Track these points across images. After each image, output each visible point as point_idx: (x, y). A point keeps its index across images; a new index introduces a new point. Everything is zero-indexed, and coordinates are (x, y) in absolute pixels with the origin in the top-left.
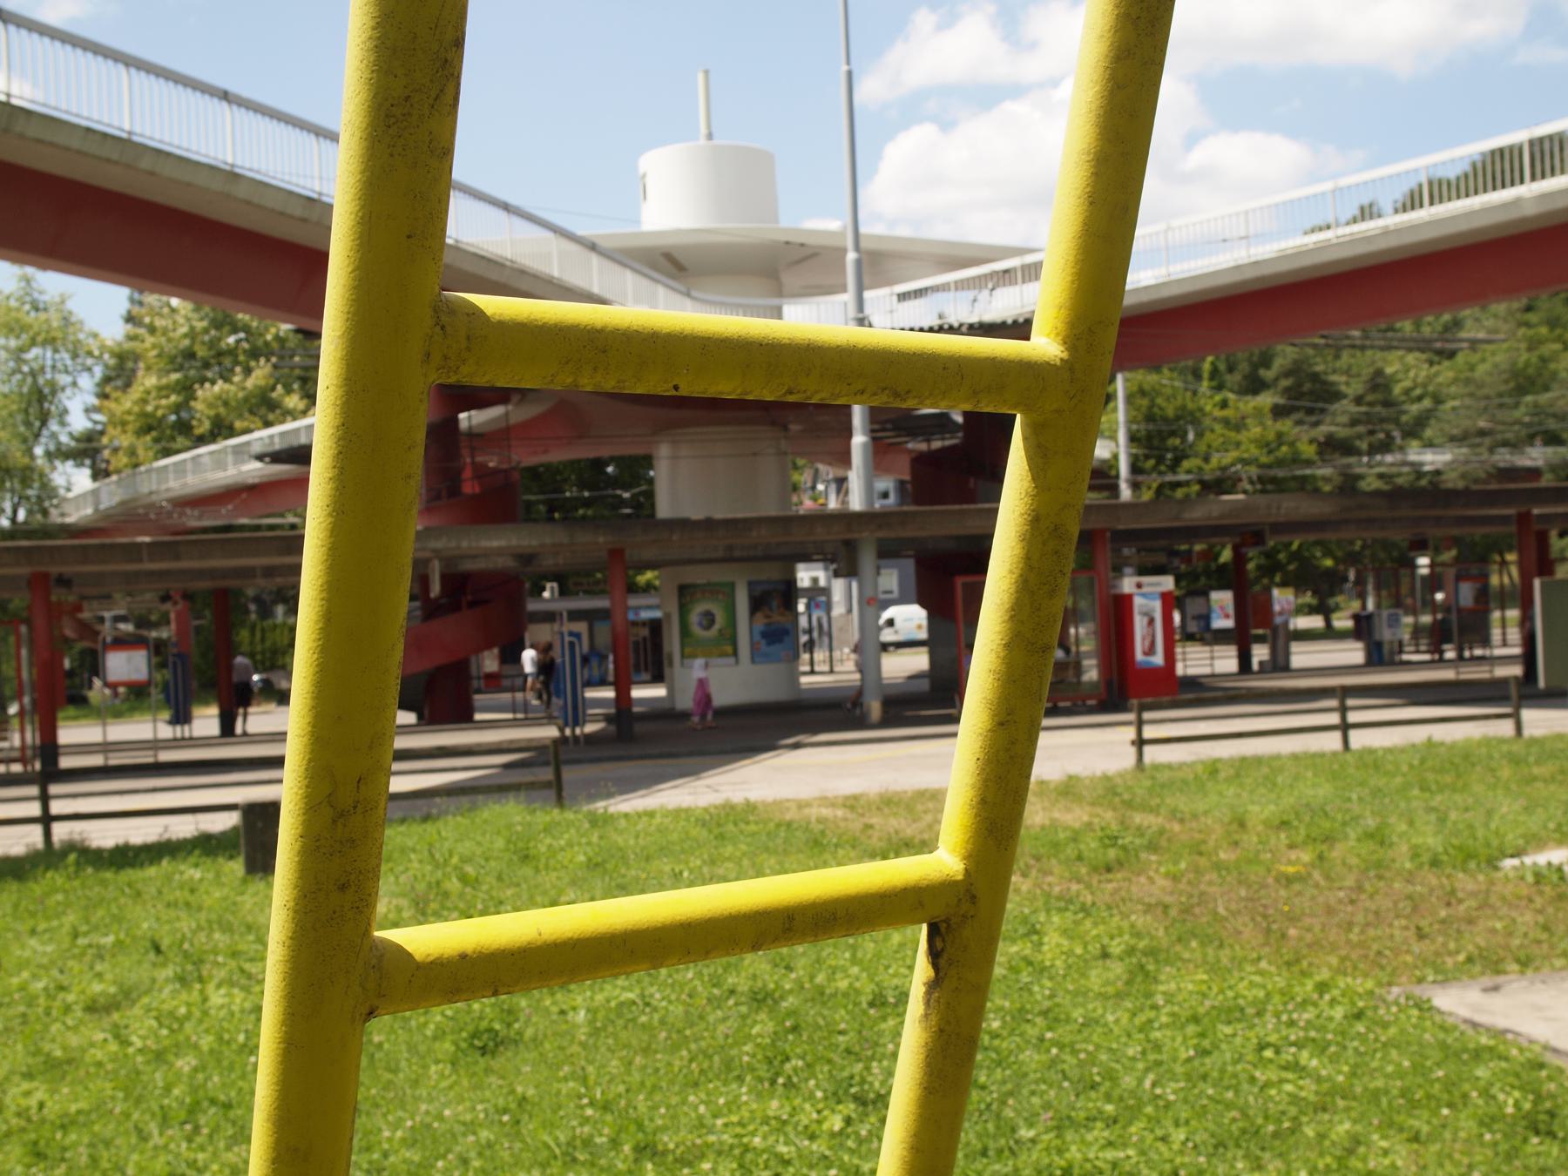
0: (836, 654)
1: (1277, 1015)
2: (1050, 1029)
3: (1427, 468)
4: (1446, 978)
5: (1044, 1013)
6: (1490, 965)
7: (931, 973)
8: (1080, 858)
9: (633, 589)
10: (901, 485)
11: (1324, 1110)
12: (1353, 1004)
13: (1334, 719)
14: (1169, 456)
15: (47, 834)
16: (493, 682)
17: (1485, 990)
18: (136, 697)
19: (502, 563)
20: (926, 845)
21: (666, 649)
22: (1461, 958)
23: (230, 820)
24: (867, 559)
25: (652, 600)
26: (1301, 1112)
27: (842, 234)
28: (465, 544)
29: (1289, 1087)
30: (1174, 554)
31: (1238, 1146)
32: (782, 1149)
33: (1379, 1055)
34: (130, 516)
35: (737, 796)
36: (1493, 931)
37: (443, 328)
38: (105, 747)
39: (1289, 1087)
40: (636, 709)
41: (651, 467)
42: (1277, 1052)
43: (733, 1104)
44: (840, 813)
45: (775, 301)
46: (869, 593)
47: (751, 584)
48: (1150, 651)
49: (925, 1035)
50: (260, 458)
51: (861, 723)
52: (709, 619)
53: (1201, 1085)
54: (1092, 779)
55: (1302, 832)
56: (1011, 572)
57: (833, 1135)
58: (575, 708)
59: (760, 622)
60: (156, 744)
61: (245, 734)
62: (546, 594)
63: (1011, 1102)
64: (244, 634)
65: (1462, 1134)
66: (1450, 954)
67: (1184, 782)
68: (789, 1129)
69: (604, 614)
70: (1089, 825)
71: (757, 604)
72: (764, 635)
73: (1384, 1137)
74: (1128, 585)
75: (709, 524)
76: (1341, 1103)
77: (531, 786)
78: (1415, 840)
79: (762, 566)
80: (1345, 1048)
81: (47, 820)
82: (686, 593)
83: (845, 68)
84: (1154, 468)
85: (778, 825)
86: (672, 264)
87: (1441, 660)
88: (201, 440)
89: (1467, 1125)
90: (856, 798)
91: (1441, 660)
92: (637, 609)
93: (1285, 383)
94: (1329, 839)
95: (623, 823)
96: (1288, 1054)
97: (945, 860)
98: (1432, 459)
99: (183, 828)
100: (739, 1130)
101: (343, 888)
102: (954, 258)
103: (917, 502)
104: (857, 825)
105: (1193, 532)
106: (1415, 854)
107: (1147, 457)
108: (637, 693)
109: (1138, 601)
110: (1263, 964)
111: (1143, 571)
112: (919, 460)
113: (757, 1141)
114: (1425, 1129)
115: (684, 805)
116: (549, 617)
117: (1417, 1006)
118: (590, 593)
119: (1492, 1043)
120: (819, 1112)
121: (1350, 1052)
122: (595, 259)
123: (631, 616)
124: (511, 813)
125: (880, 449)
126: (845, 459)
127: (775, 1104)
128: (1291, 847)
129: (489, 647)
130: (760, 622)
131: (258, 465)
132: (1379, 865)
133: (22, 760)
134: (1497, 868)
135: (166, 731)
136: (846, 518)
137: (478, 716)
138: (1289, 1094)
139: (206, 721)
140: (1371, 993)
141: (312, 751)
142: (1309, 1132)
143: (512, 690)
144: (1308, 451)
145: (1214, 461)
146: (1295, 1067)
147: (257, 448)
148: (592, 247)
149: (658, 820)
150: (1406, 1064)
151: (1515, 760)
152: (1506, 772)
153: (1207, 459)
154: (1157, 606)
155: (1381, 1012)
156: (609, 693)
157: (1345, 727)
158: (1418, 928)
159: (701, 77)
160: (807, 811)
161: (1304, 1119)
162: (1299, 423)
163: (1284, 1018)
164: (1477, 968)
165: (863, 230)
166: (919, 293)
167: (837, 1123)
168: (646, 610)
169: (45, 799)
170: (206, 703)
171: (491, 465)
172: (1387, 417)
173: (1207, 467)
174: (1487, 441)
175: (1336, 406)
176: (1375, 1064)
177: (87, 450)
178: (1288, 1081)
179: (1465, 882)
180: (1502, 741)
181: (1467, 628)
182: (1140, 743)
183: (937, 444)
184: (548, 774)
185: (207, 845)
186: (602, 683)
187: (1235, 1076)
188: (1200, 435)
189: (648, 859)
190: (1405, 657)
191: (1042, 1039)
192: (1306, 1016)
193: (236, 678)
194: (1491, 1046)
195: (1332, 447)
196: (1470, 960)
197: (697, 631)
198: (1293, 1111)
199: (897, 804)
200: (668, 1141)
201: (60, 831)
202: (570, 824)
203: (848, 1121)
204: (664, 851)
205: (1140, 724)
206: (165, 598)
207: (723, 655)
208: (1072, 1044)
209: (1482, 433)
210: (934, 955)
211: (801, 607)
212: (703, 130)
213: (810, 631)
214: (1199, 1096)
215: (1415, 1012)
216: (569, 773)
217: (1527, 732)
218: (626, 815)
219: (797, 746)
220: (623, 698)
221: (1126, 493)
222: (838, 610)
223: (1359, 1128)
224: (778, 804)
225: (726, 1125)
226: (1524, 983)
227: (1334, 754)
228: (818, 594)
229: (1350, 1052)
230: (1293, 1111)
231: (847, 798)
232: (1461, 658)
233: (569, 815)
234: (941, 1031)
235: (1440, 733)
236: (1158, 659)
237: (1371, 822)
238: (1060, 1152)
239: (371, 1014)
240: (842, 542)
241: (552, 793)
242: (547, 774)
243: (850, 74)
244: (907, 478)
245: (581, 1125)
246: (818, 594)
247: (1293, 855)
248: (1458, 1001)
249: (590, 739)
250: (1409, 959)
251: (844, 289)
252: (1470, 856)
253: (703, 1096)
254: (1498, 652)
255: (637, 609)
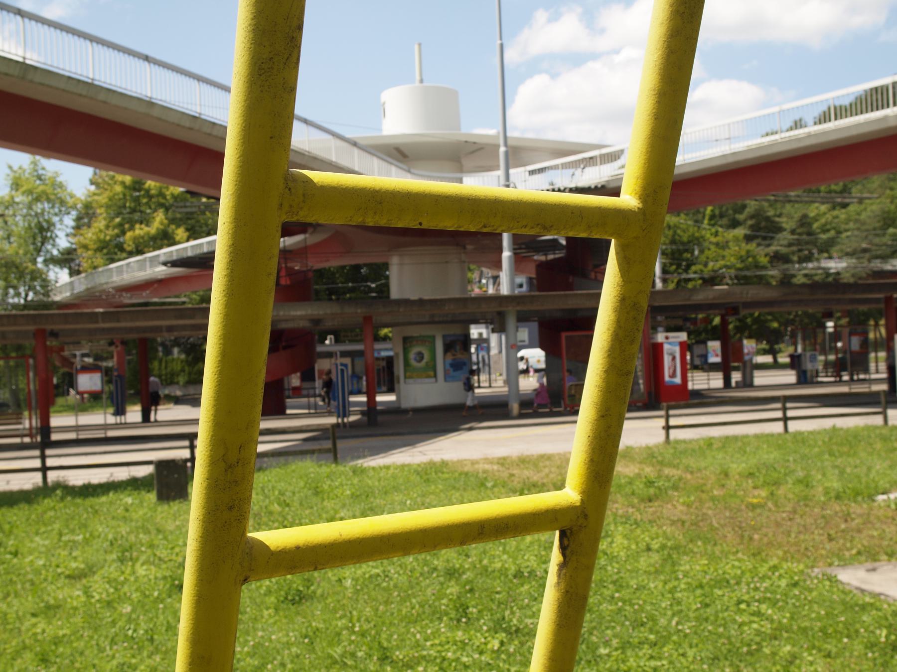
0: (493, 377)
1: (748, 584)
2: (617, 591)
3: (832, 271)
4: (845, 564)
5: (614, 583)
6: (871, 556)
7: (561, 558)
8: (633, 494)
9: (377, 339)
10: (530, 280)
11: (776, 638)
12: (792, 578)
13: (779, 414)
14: (684, 263)
15: (45, 478)
16: (297, 392)
17: (868, 570)
18: (94, 399)
19: (303, 324)
20: (560, 486)
21: (396, 373)
22: (854, 552)
23: (149, 470)
24: (511, 322)
25: (388, 345)
26: (763, 640)
27: (496, 137)
28: (281, 313)
29: (755, 626)
30: (686, 319)
31: (726, 659)
32: (465, 659)
33: (807, 608)
34: (91, 297)
35: (437, 458)
36: (872, 537)
37: (290, 189)
38: (77, 428)
39: (755, 626)
40: (379, 408)
41: (387, 269)
42: (748, 605)
43: (436, 633)
44: (495, 467)
45: (458, 175)
46: (512, 342)
47: (444, 337)
48: (673, 375)
49: (557, 594)
50: (165, 264)
51: (507, 416)
52: (420, 356)
53: (705, 624)
54: (640, 448)
55: (761, 479)
56: (608, 329)
57: (493, 651)
58: (344, 406)
59: (450, 358)
60: (106, 427)
61: (156, 421)
62: (327, 342)
63: (595, 632)
64: (156, 364)
65: (856, 653)
66: (848, 550)
67: (693, 450)
68: (468, 648)
69: (361, 353)
70: (639, 475)
71: (448, 348)
72: (452, 365)
73: (811, 655)
74: (660, 337)
75: (421, 302)
76: (785, 635)
77: (320, 451)
78: (826, 485)
79: (451, 327)
80: (787, 603)
81: (44, 469)
82: (407, 341)
83: (499, 42)
84: (675, 271)
85: (460, 474)
86: (400, 154)
87: (841, 381)
88: (131, 254)
89: (858, 647)
90: (505, 459)
91: (841, 381)
92: (380, 350)
93: (750, 222)
94: (777, 483)
95: (371, 473)
96: (754, 607)
97: (570, 494)
98: (835, 265)
99: (122, 474)
100: (439, 648)
101: (231, 508)
102: (561, 150)
103: (540, 290)
104: (505, 474)
105: (698, 307)
106: (826, 492)
107: (671, 264)
108: (380, 398)
109: (666, 347)
110: (740, 555)
111: (668, 329)
112: (541, 266)
113: (450, 655)
114: (834, 650)
115: (406, 463)
116: (329, 355)
117: (829, 579)
118: (353, 341)
119: (872, 601)
120: (485, 638)
121: (790, 606)
122: (356, 151)
123: (376, 355)
124: (308, 467)
125: (518, 260)
126: (498, 265)
127: (460, 633)
128: (755, 488)
129: (295, 372)
130: (450, 358)
131: (164, 268)
132: (806, 498)
133: (30, 435)
134: (874, 501)
135: (111, 420)
136: (499, 299)
137: (288, 412)
138: (755, 630)
139: (134, 414)
140: (802, 572)
141: (214, 431)
142: (767, 651)
143: (308, 396)
144: (764, 260)
145: (711, 264)
146: (758, 614)
147: (162, 259)
148: (355, 144)
149: (391, 471)
150: (823, 612)
151: (884, 439)
152: (879, 445)
153: (706, 265)
154: (677, 350)
155: (808, 583)
156: (363, 399)
157: (785, 419)
158: (829, 535)
159: (416, 47)
160: (476, 466)
161: (764, 644)
162: (759, 245)
163: (752, 586)
164: (863, 558)
165: (509, 134)
166: (541, 171)
167: (496, 644)
168: (384, 351)
169: (43, 457)
170: (134, 403)
171: (296, 268)
172: (811, 242)
173: (706, 270)
174: (867, 255)
175: (780, 236)
176: (804, 613)
177: (67, 259)
178: (754, 622)
179: (855, 509)
180: (876, 427)
181: (855, 363)
182: (668, 428)
183: (551, 257)
184: (328, 445)
185: (134, 484)
186: (359, 392)
187: (724, 619)
188: (702, 252)
189: (386, 493)
190: (820, 379)
191: (613, 597)
192: (764, 585)
193: (151, 389)
194: (872, 603)
195: (778, 258)
196: (859, 553)
197: (413, 363)
198: (758, 639)
199: (529, 462)
200: (398, 654)
201: (52, 476)
202: (342, 473)
203: (502, 643)
204: (396, 489)
205: (667, 417)
206: (111, 344)
207: (428, 377)
208: (630, 600)
209: (865, 251)
210: (563, 548)
211: (473, 350)
212: (418, 78)
213: (478, 363)
214: (703, 630)
215: (827, 583)
216: (341, 444)
217: (890, 423)
218: (373, 468)
219: (470, 429)
220: (371, 401)
221: (659, 285)
222: (494, 351)
223: (796, 649)
224: (461, 462)
225: (432, 645)
226: (890, 567)
227: (779, 435)
228: (483, 343)
229: (790, 606)
230: (758, 639)
231: (500, 459)
232: (852, 380)
233: (341, 468)
234: (567, 592)
235: (840, 422)
236: (678, 380)
237: (801, 474)
238: (624, 662)
239: (245, 580)
240: (496, 313)
241: (331, 455)
242: (328, 444)
243: (502, 46)
244: (534, 276)
245: (350, 645)
246: (483, 343)
247: (756, 492)
248: (852, 577)
249: (353, 425)
250: (823, 552)
251: (497, 168)
252: (857, 494)
253: (419, 628)
254: (874, 376)
255: (380, 350)
